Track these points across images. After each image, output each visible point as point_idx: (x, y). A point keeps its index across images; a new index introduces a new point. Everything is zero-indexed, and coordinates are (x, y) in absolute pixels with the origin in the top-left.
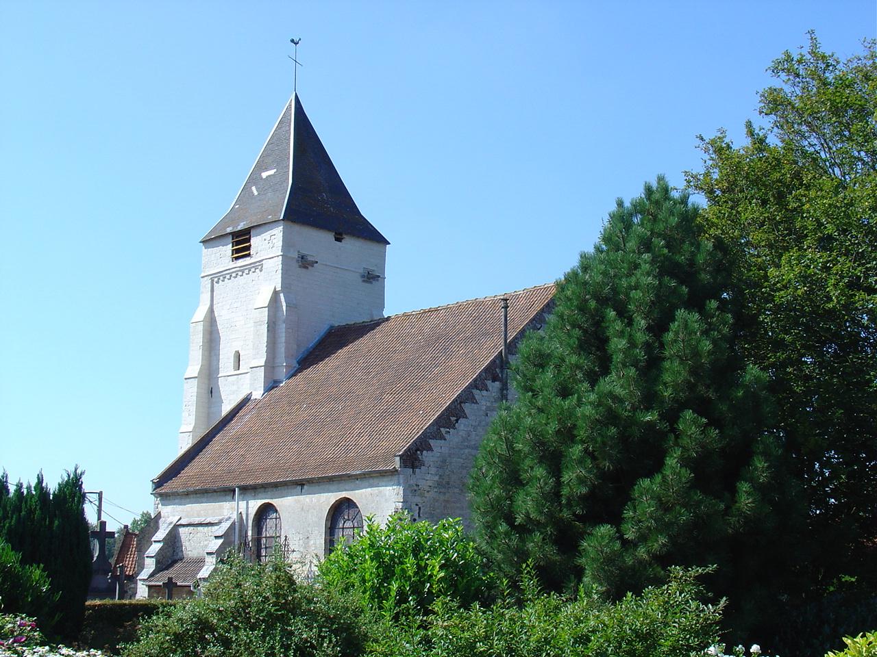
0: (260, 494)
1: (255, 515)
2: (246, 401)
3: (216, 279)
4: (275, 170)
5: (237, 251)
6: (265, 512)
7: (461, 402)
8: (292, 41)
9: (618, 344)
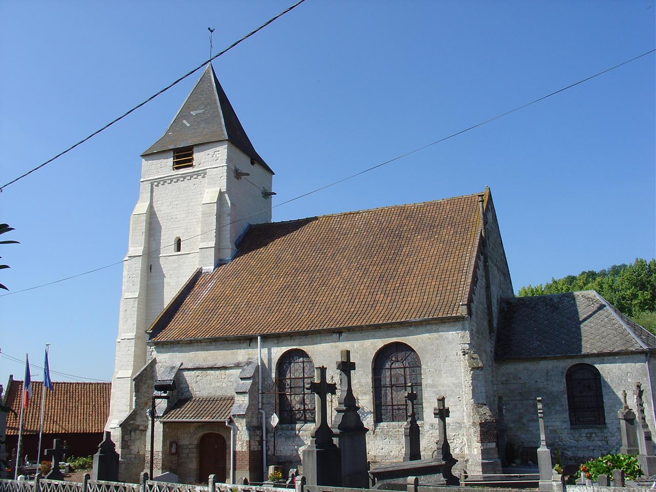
1: (279, 360)
2: (198, 274)
5: (177, 163)
6: (285, 360)
8: (209, 29)
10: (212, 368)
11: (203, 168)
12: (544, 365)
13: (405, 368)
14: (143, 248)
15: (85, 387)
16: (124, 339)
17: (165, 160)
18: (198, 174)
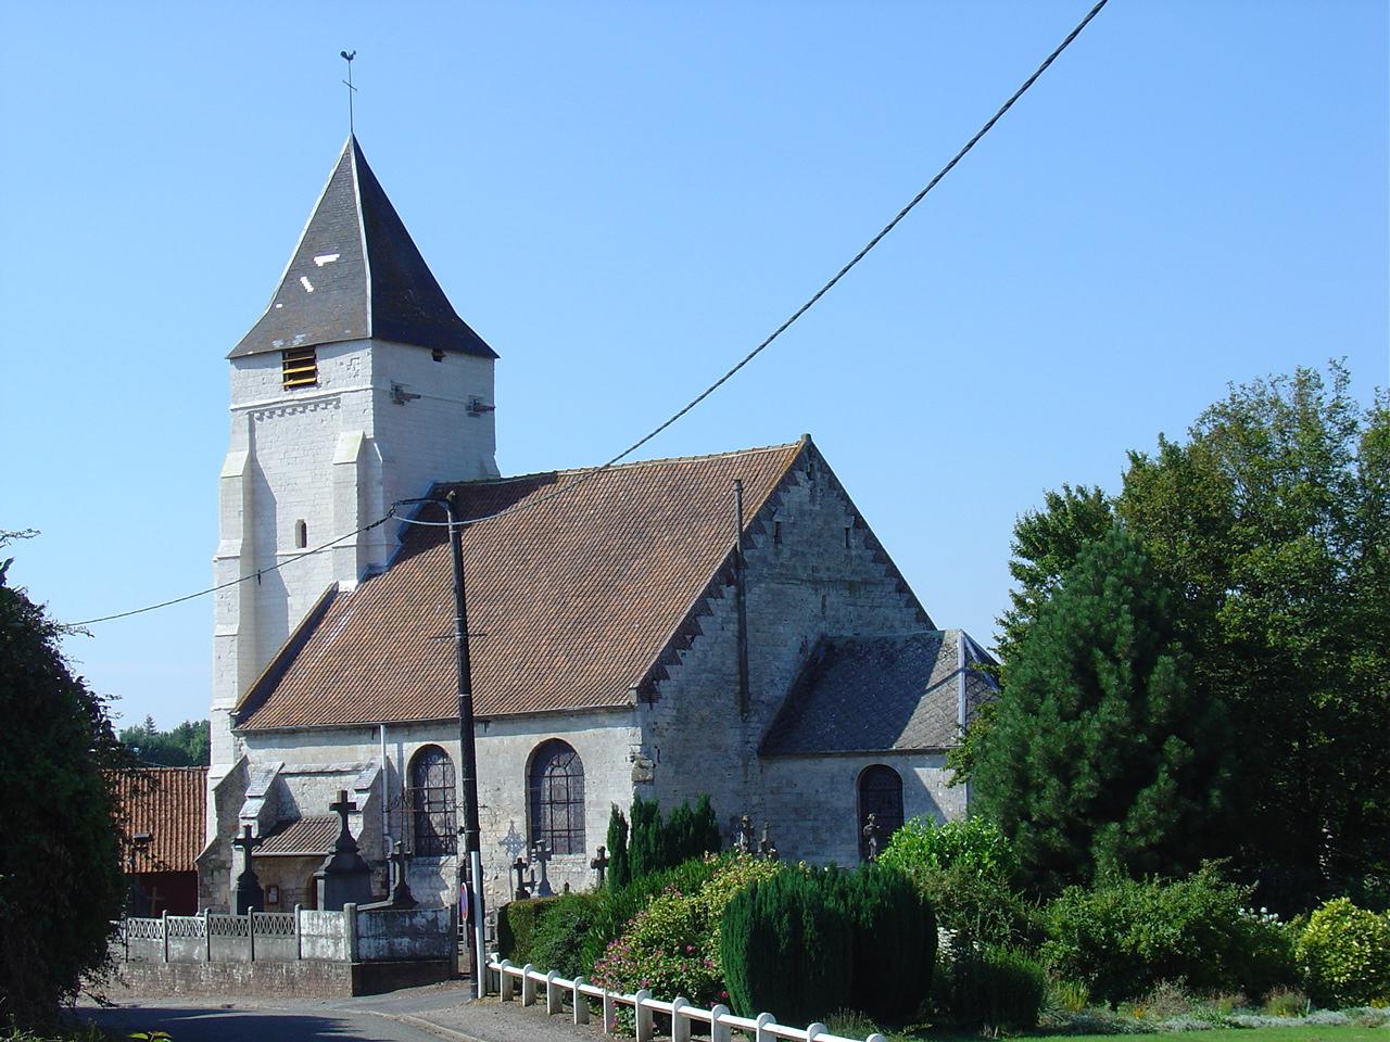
0: (418, 734)
2: (331, 596)
3: (256, 415)
4: (338, 256)
5: (292, 376)
6: (423, 758)
7: (696, 615)
8: (344, 54)
9: (1109, 680)
10: (322, 773)
11: (334, 391)
12: (831, 765)
13: (567, 776)
14: (241, 541)
15: (191, 778)
16: (220, 709)
17: (269, 370)
18: (326, 401)
